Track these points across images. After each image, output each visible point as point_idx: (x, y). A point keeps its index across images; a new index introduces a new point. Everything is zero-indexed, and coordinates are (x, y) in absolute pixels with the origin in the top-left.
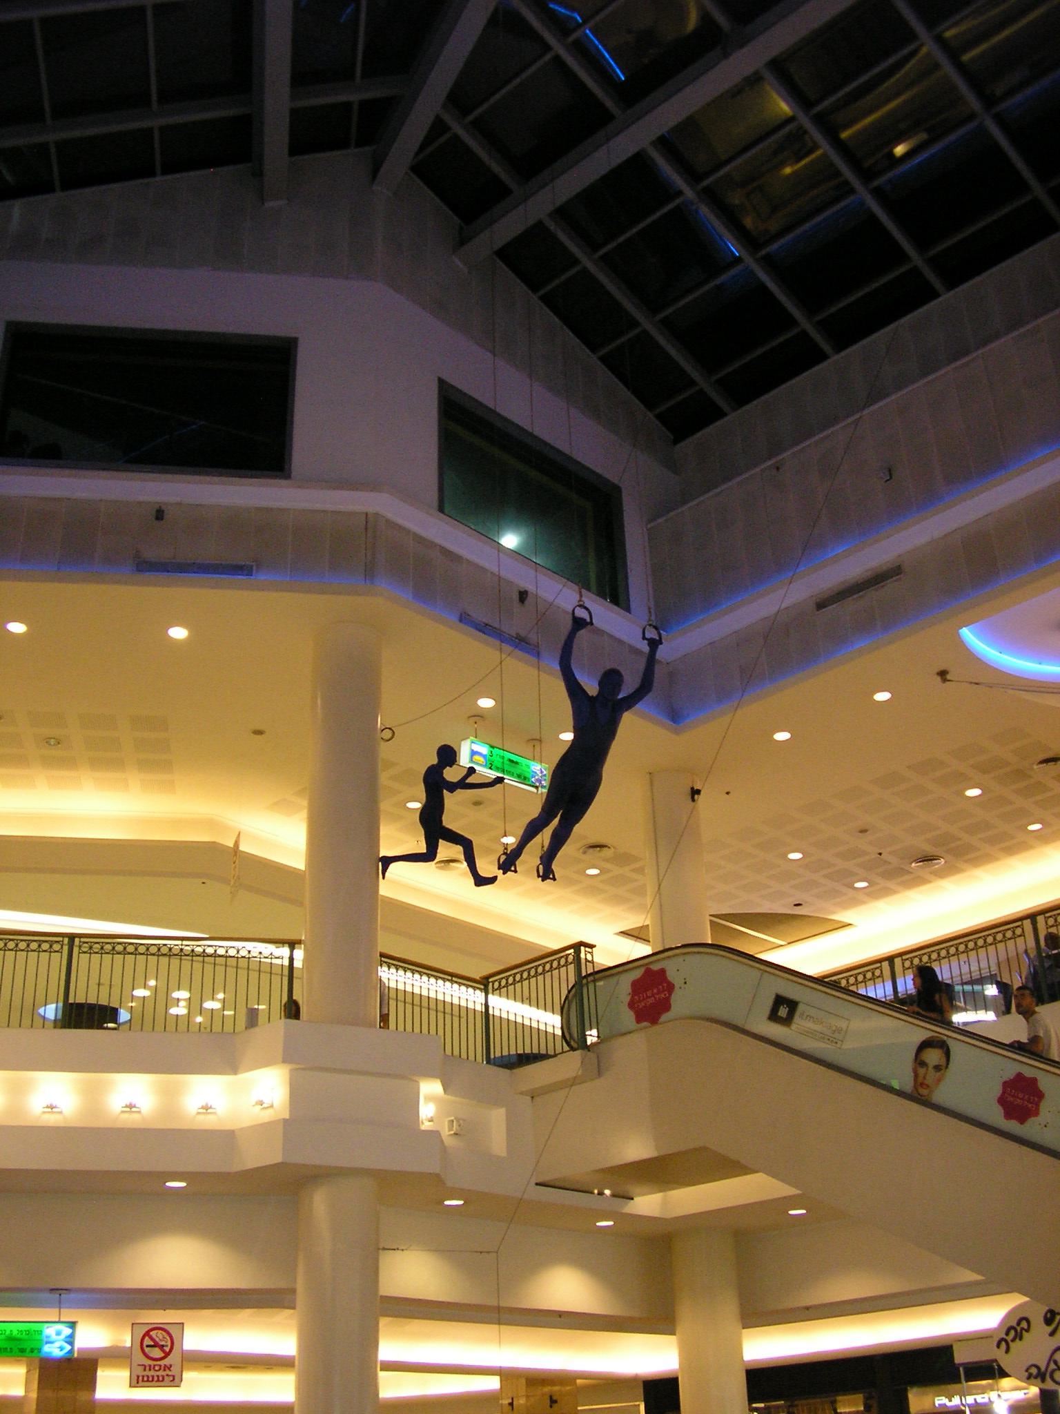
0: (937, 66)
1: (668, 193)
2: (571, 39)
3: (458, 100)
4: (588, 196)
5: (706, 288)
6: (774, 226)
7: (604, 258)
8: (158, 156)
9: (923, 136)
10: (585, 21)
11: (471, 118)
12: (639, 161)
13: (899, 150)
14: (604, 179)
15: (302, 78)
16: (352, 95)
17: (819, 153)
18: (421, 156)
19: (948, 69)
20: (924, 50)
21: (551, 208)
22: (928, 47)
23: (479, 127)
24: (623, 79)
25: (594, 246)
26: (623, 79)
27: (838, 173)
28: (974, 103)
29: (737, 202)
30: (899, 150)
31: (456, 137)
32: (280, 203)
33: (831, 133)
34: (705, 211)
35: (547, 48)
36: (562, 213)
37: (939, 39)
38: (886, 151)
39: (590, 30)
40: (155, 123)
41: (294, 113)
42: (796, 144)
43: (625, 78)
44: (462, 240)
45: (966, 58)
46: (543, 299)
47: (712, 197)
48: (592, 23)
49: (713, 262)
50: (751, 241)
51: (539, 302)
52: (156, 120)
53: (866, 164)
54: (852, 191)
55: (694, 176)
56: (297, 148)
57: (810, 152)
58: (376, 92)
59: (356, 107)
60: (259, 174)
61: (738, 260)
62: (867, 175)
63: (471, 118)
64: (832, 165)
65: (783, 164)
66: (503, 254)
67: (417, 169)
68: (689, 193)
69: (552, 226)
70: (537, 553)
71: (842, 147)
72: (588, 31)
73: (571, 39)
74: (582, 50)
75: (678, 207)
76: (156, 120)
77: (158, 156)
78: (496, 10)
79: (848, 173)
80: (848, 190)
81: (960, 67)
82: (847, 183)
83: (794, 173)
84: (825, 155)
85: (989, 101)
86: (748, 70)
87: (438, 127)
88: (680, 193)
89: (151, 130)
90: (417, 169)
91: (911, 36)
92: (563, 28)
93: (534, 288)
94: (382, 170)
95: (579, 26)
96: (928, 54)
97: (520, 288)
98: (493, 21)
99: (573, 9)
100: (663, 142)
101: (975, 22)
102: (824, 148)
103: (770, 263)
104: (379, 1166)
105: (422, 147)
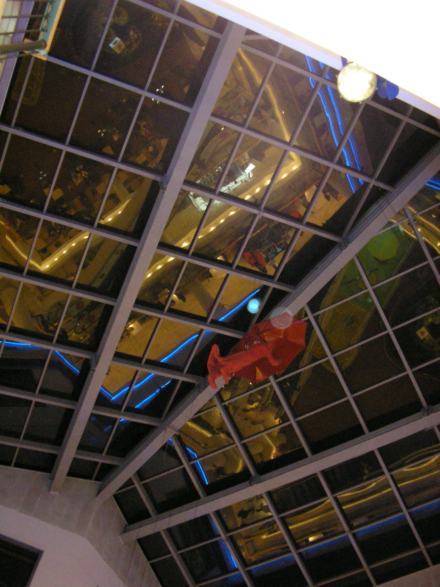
0: (332, 508)
1: (213, 534)
2: (192, 463)
3: (141, 474)
4: (181, 527)
5: (220, 578)
6: (254, 558)
7: (181, 554)
8: (14, 459)
9: (322, 535)
10: (198, 458)
11: (144, 482)
12: (205, 519)
13: (311, 539)
14: (190, 522)
15: (82, 447)
16: (101, 459)
17: (279, 532)
18: (120, 491)
19: (337, 510)
20: (328, 501)
21: (167, 527)
22: (330, 500)
23: (146, 487)
24: (207, 484)
25: (178, 548)
26: (207, 484)
27: (285, 543)
28: (346, 527)
29: (241, 545)
30: (311, 539)
31: (135, 489)
32: (56, 493)
33: (286, 526)
34: (228, 546)
35: (181, 463)
36: (169, 531)
37: (336, 499)
38: (306, 538)
39: (199, 462)
40: (19, 446)
41: (75, 460)
42: (270, 527)
43: (208, 483)
44: (125, 531)
45: (344, 508)
46: (152, 565)
47: (232, 540)
48: (202, 459)
49: (226, 568)
50: (244, 563)
51: (150, 566)
52: (20, 445)
53: (297, 542)
54: (290, 551)
55: (227, 530)
56: (71, 474)
57: (275, 531)
58: (108, 461)
59: (99, 465)
60: (52, 479)
61: (237, 569)
62: (297, 546)
63: (144, 482)
64: (284, 539)
65: (263, 534)
66: (140, 541)
67: (115, 496)
68: (223, 536)
69: (164, 536)
70: (213, 405)
71: (288, 531)
72: (198, 462)
73: (192, 463)
74: (194, 467)
75: (217, 541)
76: (20, 445)
77: (14, 459)
78: (166, 444)
79: (289, 543)
80: (287, 550)
81: (342, 511)
82: (288, 547)
83: (267, 539)
84: (281, 534)
85: (351, 527)
86: (258, 493)
87: (129, 482)
88: (219, 535)
89: (15, 448)
90: (115, 496)
91: (324, 495)
92: (190, 458)
93: (149, 559)
94: (103, 492)
95: (195, 459)
96: (330, 503)
97: (143, 557)
98: (163, 448)
99: (195, 452)
100: (218, 513)
101: (350, 494)
102: (282, 531)
103: (249, 573)
104: (123, 483)
105: (121, 489)
